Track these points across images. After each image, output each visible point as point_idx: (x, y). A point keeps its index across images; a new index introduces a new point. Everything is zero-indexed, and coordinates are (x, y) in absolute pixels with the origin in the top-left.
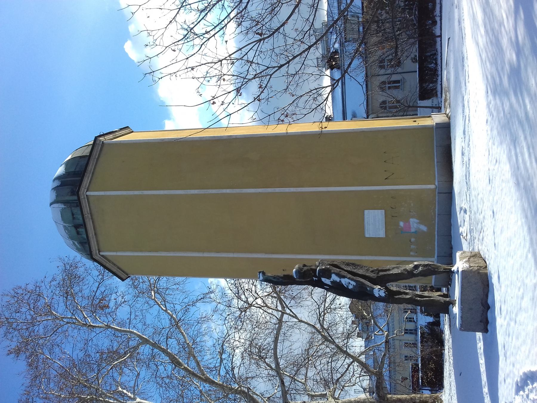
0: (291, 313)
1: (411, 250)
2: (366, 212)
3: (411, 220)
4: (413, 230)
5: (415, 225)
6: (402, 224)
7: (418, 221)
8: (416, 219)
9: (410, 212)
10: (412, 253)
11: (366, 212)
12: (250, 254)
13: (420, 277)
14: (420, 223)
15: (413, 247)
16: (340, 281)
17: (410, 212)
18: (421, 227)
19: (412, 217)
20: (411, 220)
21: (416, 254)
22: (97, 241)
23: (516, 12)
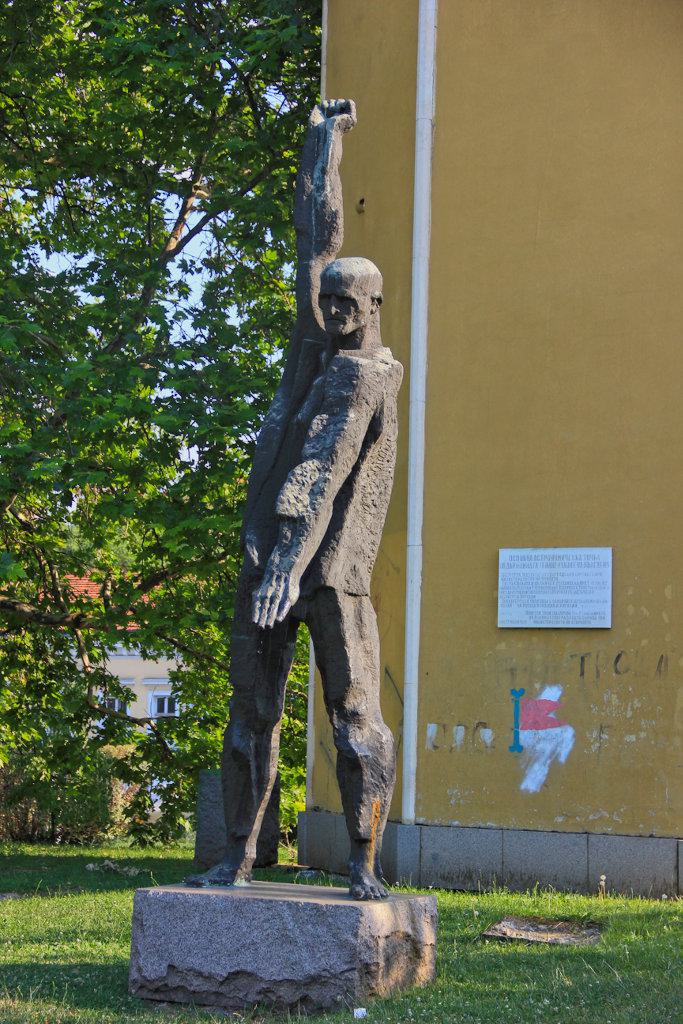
0: (185, 232)
1: (444, 728)
2: (605, 554)
3: (568, 733)
4: (526, 737)
5: (547, 747)
6: (552, 694)
7: (562, 759)
8: (571, 753)
9: (601, 730)
10: (432, 729)
11: (605, 554)
12: (421, 37)
13: (335, 752)
14: (554, 766)
15: (460, 733)
16: (174, 261)
17: (601, 730)
18: (536, 767)
19: (579, 738)
20: (568, 733)
21: (429, 746)
22: (678, 860)
23: (330, 713)
